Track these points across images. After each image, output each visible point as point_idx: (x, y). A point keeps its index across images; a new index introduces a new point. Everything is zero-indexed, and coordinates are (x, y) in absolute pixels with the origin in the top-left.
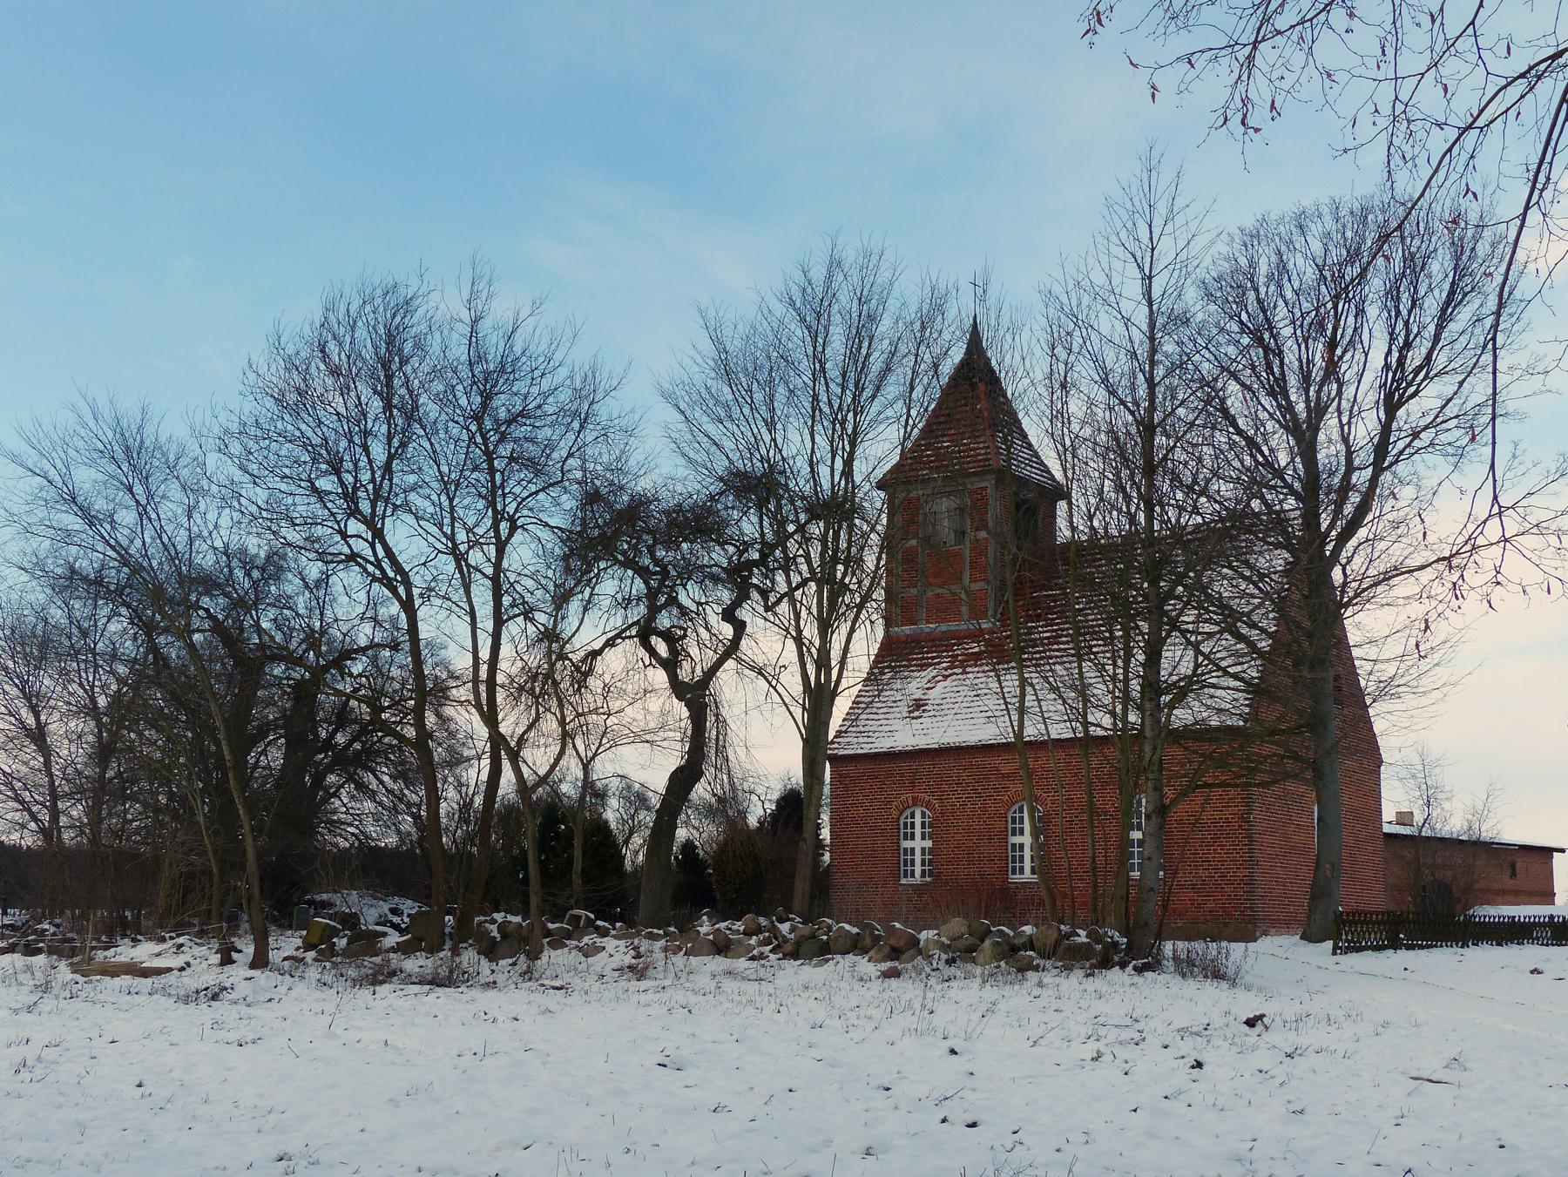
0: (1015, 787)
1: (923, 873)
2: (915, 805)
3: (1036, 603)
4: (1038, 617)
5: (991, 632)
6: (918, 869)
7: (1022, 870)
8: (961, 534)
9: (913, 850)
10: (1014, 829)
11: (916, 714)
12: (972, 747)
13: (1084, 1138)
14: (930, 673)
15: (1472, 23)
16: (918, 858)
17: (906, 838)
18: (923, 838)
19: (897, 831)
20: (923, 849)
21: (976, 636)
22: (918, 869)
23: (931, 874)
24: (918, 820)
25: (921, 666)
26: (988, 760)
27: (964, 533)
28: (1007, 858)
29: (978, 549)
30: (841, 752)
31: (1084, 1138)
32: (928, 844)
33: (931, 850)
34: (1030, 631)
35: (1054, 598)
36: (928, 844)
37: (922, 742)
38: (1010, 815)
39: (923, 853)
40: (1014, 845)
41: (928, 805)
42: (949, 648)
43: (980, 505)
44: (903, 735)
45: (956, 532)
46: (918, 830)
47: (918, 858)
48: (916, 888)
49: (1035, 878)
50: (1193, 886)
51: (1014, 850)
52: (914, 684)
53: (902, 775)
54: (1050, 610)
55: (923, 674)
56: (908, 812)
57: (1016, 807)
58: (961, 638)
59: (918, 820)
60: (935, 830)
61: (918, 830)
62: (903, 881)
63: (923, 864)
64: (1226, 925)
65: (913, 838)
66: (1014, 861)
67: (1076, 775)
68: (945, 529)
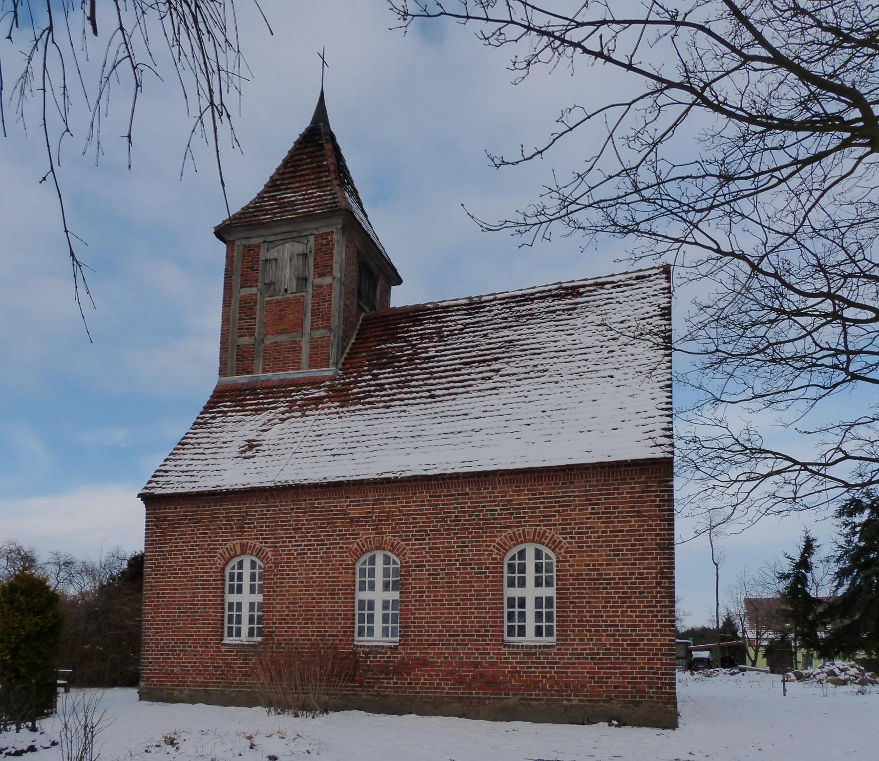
0: (365, 534)
1: (251, 633)
2: (243, 553)
3: (382, 354)
4: (385, 366)
5: (333, 379)
6: (245, 627)
7: (371, 631)
8: (303, 280)
9: (239, 605)
10: (362, 583)
11: (249, 454)
12: (316, 486)
13: (248, 743)
14: (265, 416)
15: (630, 104)
16: (245, 614)
17: (231, 591)
18: (252, 591)
19: (220, 583)
20: (252, 605)
21: (315, 383)
22: (245, 627)
23: (260, 633)
24: (247, 571)
25: (256, 410)
26: (333, 502)
27: (306, 279)
28: (352, 617)
29: (322, 295)
30: (158, 492)
31: (248, 743)
32: (258, 598)
33: (261, 606)
34: (375, 377)
35: (400, 349)
36: (258, 598)
37: (254, 481)
38: (358, 566)
39: (252, 608)
40: (362, 602)
41: (259, 553)
42: (288, 394)
43: (324, 250)
44: (235, 475)
45: (298, 279)
46: (246, 583)
47: (245, 614)
48: (241, 648)
49: (393, 640)
50: (594, 656)
51: (362, 608)
52: (248, 426)
53: (229, 519)
54: (398, 359)
55: (257, 417)
56: (235, 562)
57: (366, 557)
58: (299, 385)
59: (247, 571)
60: (267, 583)
61: (246, 583)
62: (227, 640)
63: (251, 621)
64: (637, 704)
65: (240, 591)
66: (361, 621)
67: (443, 520)
68: (287, 276)
